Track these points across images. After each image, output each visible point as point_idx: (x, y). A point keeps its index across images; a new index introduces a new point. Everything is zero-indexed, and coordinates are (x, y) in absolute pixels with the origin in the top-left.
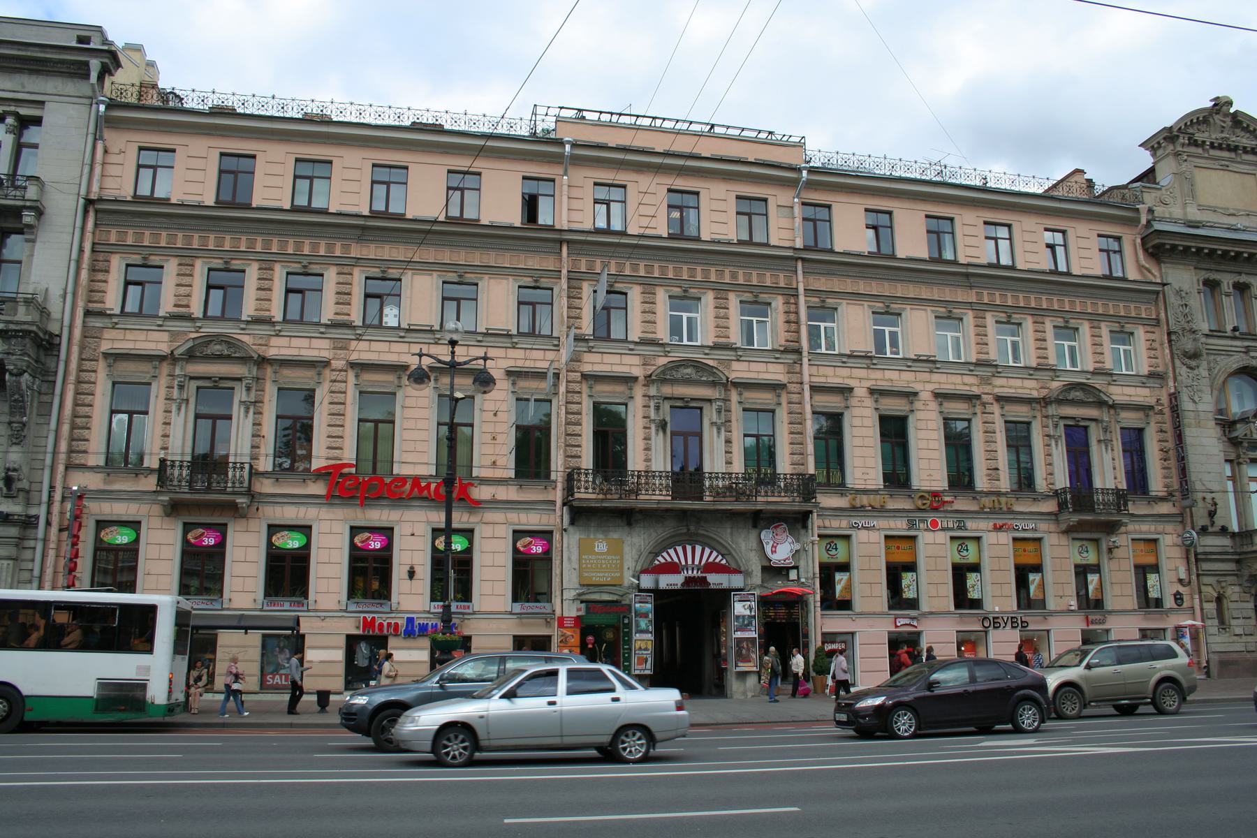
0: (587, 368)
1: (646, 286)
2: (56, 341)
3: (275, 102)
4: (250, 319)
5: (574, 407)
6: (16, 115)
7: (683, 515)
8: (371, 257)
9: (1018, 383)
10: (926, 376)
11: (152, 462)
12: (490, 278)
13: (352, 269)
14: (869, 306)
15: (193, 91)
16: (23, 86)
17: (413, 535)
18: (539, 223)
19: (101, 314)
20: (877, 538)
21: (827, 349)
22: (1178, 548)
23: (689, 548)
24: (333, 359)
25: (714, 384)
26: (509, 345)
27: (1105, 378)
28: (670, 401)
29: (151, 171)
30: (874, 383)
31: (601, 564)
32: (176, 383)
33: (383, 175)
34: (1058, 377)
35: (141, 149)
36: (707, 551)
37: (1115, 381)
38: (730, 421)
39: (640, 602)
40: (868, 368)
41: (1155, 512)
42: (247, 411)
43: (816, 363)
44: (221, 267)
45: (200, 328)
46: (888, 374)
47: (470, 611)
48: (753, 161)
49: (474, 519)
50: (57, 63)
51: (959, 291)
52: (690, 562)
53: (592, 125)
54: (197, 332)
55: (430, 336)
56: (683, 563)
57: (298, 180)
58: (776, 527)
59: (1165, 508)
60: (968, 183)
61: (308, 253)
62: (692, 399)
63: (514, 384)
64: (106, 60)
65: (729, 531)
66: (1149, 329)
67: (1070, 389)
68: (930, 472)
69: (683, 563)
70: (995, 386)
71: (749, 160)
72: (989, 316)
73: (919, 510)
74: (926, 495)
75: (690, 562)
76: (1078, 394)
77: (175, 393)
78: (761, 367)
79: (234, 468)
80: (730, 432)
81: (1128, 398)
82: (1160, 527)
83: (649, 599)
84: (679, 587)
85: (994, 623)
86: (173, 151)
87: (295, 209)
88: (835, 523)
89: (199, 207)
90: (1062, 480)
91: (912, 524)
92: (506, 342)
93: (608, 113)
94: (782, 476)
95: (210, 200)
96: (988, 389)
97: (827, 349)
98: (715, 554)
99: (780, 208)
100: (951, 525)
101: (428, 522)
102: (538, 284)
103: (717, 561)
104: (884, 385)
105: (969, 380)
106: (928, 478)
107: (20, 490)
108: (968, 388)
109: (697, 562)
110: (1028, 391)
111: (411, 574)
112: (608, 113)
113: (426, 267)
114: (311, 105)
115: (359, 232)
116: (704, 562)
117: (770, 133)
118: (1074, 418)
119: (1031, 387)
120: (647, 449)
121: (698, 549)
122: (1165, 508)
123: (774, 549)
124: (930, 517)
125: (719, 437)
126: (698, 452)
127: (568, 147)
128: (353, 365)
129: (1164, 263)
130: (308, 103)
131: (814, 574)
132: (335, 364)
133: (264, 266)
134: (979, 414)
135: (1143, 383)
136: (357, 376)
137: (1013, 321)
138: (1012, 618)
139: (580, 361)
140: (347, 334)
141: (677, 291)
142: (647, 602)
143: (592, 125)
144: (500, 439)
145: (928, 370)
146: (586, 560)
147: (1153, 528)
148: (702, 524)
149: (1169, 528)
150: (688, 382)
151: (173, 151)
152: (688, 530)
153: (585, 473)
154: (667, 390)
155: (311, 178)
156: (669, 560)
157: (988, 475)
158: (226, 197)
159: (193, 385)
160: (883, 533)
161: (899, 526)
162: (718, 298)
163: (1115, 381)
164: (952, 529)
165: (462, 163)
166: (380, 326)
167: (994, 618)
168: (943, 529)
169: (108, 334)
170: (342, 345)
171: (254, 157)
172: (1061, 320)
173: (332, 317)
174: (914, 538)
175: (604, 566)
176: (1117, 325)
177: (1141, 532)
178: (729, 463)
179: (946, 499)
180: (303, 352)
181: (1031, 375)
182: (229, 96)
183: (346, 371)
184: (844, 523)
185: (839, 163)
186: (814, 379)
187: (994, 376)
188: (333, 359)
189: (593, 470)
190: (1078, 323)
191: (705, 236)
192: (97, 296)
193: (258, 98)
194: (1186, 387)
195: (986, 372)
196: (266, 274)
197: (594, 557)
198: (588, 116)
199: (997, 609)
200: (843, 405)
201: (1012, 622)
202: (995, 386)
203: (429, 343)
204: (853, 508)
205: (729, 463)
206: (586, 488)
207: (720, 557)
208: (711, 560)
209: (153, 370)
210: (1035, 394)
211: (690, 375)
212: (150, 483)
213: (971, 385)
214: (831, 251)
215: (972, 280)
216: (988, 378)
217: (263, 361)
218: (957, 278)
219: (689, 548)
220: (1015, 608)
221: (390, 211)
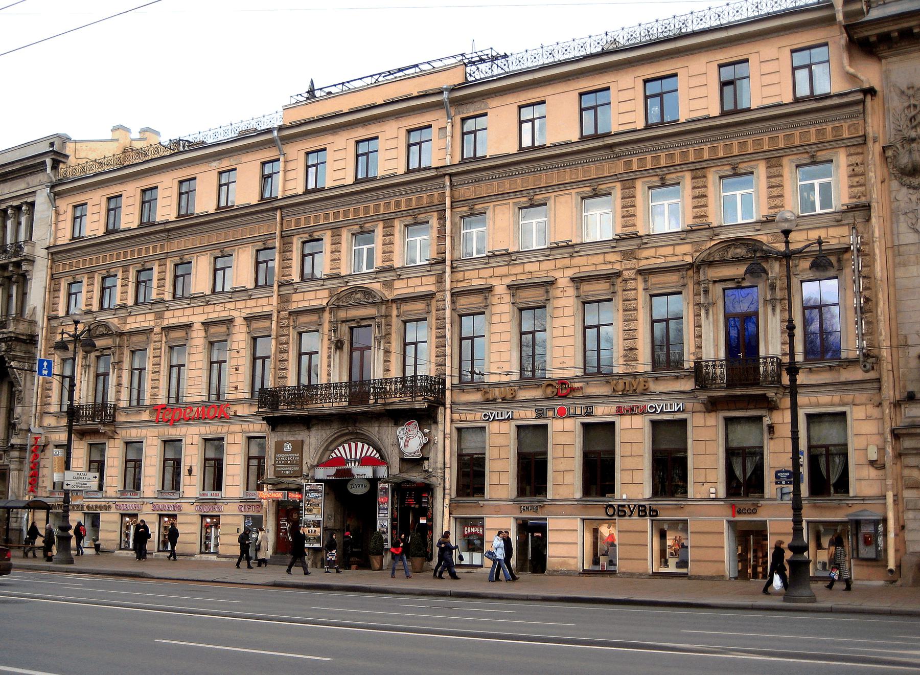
0: (294, 307)
1: (333, 230)
2: (36, 339)
4: (326, 277)
5: (284, 339)
6: (26, 203)
8: (592, 177)
9: (669, 250)
10: (566, 262)
11: (689, 364)
12: (239, 248)
13: (634, 183)
14: (578, 193)
15: (728, 4)
16: (28, 184)
17: (192, 444)
19: (56, 317)
20: (509, 429)
22: (811, 425)
23: (353, 445)
24: (438, 292)
25: (374, 304)
26: (247, 298)
28: (721, 283)
29: (592, 111)
30: (577, 270)
31: (288, 461)
32: (702, 290)
33: (654, 88)
34: (718, 235)
35: (720, 66)
36: (366, 446)
37: (577, 252)
38: (390, 334)
40: (509, 264)
41: (843, 379)
42: (774, 310)
43: (462, 269)
45: (347, 282)
46: (528, 267)
47: (220, 497)
48: (417, 94)
49: (225, 430)
50: (5, 174)
51: (606, 165)
52: (353, 457)
53: (304, 105)
54: (346, 286)
55: (162, 305)
56: (349, 457)
58: (409, 424)
59: (857, 374)
60: (567, 57)
61: (693, 160)
62: (362, 319)
63: (578, 289)
64: (53, 157)
65: (377, 429)
66: (852, 150)
67: (729, 247)
70: (641, 259)
72: (397, 223)
73: (548, 399)
74: (554, 383)
75: (353, 457)
76: (738, 251)
77: (702, 299)
78: (417, 281)
79: (765, 363)
80: (389, 343)
82: (848, 397)
85: (619, 510)
86: (675, 75)
87: (583, 139)
88: (470, 417)
89: (707, 118)
91: (540, 414)
92: (243, 296)
93: (340, 84)
94: (419, 377)
95: (715, 111)
96: (630, 264)
100: (578, 412)
101: (158, 437)
102: (267, 246)
105: (610, 257)
107: (21, 430)
108: (609, 266)
109: (358, 457)
110: (680, 258)
111: (190, 472)
112: (340, 84)
113: (201, 250)
114: (622, 34)
115: (166, 234)
116: (368, 454)
117: (462, 55)
118: (733, 280)
120: (329, 366)
121: (360, 445)
122: (857, 374)
123: (406, 443)
124: (559, 405)
125: (707, 317)
127: (275, 133)
128: (640, 272)
129: (886, 58)
131: (444, 464)
132: (626, 274)
133: (852, 152)
134: (620, 293)
135: (838, 221)
136: (645, 281)
137: (668, 183)
138: (639, 506)
139: (289, 302)
141: (356, 228)
143: (304, 105)
144: (241, 369)
146: (278, 457)
147: (837, 399)
148: (357, 425)
149: (862, 397)
150: (358, 305)
151: (746, 61)
153: (279, 390)
154: (342, 314)
155: (809, 66)
156: (339, 455)
157: (625, 356)
158: (729, 106)
159: (719, 288)
160: (514, 423)
161: (527, 416)
163: (577, 252)
164: (580, 416)
166: (313, 278)
167: (619, 506)
168: (570, 416)
169: (295, 297)
170: (159, 316)
172: (727, 168)
173: (846, 200)
174: (545, 427)
175: (289, 462)
176: (806, 156)
177: (818, 405)
178: (387, 370)
179: (577, 385)
181: (430, 271)
183: (635, 279)
184: (479, 416)
185: (660, 30)
186: (455, 285)
187: (639, 248)
188: (438, 292)
189: (726, 360)
190: (751, 167)
192: (287, 271)
194: (906, 213)
195: (388, 276)
196: (700, 182)
197: (283, 455)
198: (334, 90)
199: (624, 497)
200: (545, 298)
201: (639, 511)
202: (641, 259)
204: (487, 401)
205: (387, 370)
206: (396, 394)
207: (375, 452)
209: (682, 280)
210: (689, 259)
211: (359, 299)
212: (688, 385)
213: (614, 262)
215: (617, 150)
216: (632, 251)
217: (121, 334)
218: (602, 152)
219: (353, 445)
220: (647, 492)
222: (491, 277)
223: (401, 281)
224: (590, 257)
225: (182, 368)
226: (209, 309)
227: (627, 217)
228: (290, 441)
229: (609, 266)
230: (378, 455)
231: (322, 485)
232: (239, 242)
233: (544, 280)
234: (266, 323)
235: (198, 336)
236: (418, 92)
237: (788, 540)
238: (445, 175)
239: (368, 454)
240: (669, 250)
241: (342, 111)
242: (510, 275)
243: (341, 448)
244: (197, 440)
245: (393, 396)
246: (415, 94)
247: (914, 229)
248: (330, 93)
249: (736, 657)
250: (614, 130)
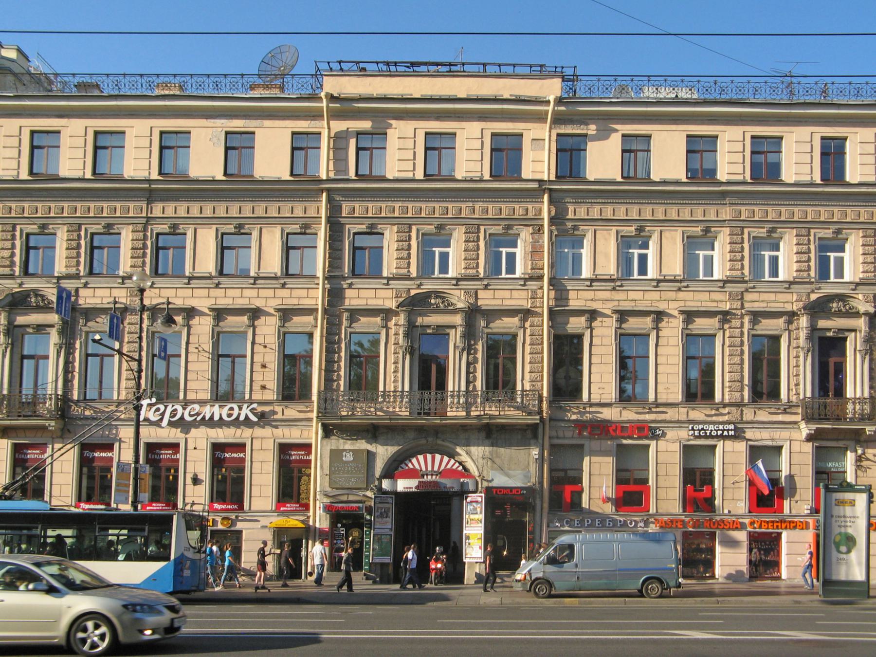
1: (400, 226)
3: (617, 84)
7: (421, 430)
10: (672, 295)
18: (590, 177)
21: (705, 276)
27: (808, 286)
39: (380, 503)
44: (299, 231)
46: (632, 295)
52: (430, 468)
57: (295, 152)
68: (601, 385)
69: (424, 469)
71: (505, 97)
75: (430, 468)
81: (699, 304)
83: (390, 500)
84: (414, 490)
90: (806, 389)
93: (494, 64)
97: (705, 276)
98: (452, 461)
99: (535, 142)
103: (454, 467)
104: (627, 306)
106: (665, 391)
109: (436, 469)
110: (782, 305)
112: (494, 64)
116: (442, 467)
119: (784, 300)
126: (19, 371)
130: (745, 84)
140: (740, 287)
142: (388, 503)
145: (610, 288)
148: (439, 435)
152: (427, 441)
162: (469, 232)
165: (237, 124)
171: (189, 133)
180: (370, 302)
182: (662, 82)
191: (654, 177)
193: (753, 84)
203: (209, 288)
206: (451, 408)
208: (449, 466)
214: (383, 179)
219: (429, 456)
221: (373, 174)
222: (592, 300)
223: (487, 291)
224: (696, 293)
225: (41, 361)
226: (219, 292)
227: (733, 261)
228: (350, 450)
229: (715, 304)
230: (461, 468)
231: (481, 496)
232: (266, 220)
233: (648, 309)
234: (310, 319)
235: (203, 326)
236: (511, 95)
237: (58, 567)
238: (322, 191)
239: (442, 467)
240: (772, 297)
241: (412, 95)
242: (612, 300)
243: (421, 457)
244: (270, 444)
245: (454, 409)
246: (506, 96)
247: (141, 312)
248: (364, 69)
249: (741, 637)
250: (390, 176)
